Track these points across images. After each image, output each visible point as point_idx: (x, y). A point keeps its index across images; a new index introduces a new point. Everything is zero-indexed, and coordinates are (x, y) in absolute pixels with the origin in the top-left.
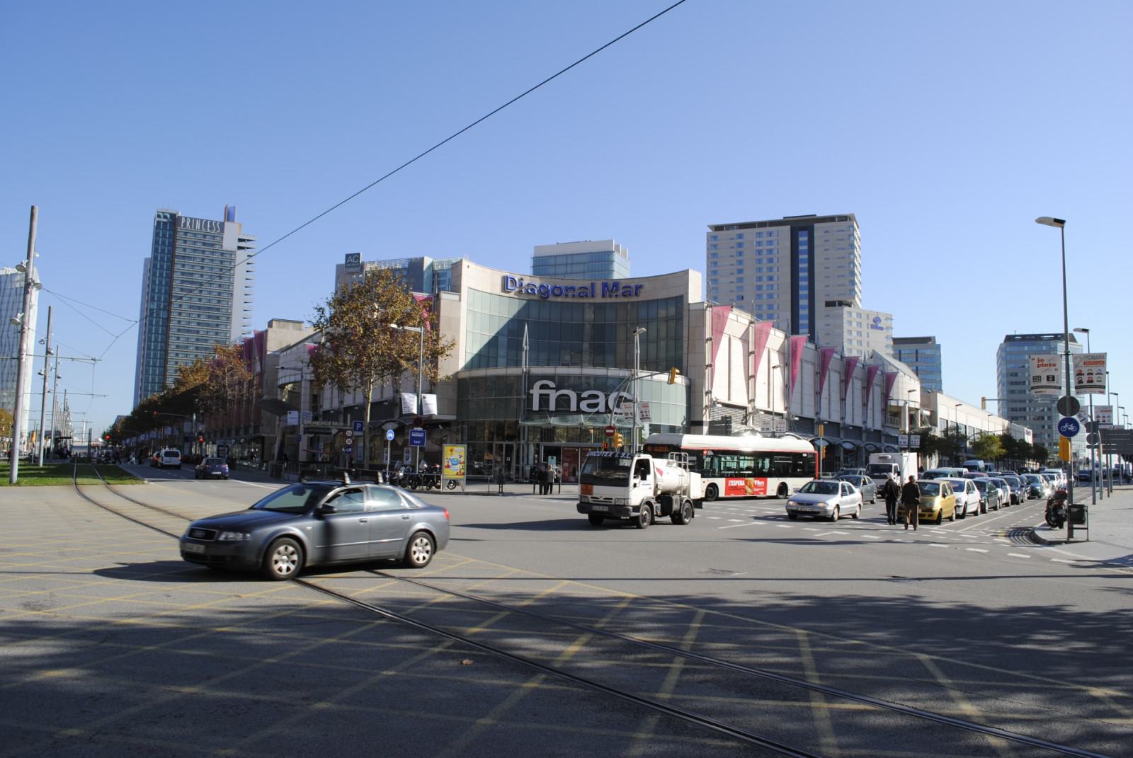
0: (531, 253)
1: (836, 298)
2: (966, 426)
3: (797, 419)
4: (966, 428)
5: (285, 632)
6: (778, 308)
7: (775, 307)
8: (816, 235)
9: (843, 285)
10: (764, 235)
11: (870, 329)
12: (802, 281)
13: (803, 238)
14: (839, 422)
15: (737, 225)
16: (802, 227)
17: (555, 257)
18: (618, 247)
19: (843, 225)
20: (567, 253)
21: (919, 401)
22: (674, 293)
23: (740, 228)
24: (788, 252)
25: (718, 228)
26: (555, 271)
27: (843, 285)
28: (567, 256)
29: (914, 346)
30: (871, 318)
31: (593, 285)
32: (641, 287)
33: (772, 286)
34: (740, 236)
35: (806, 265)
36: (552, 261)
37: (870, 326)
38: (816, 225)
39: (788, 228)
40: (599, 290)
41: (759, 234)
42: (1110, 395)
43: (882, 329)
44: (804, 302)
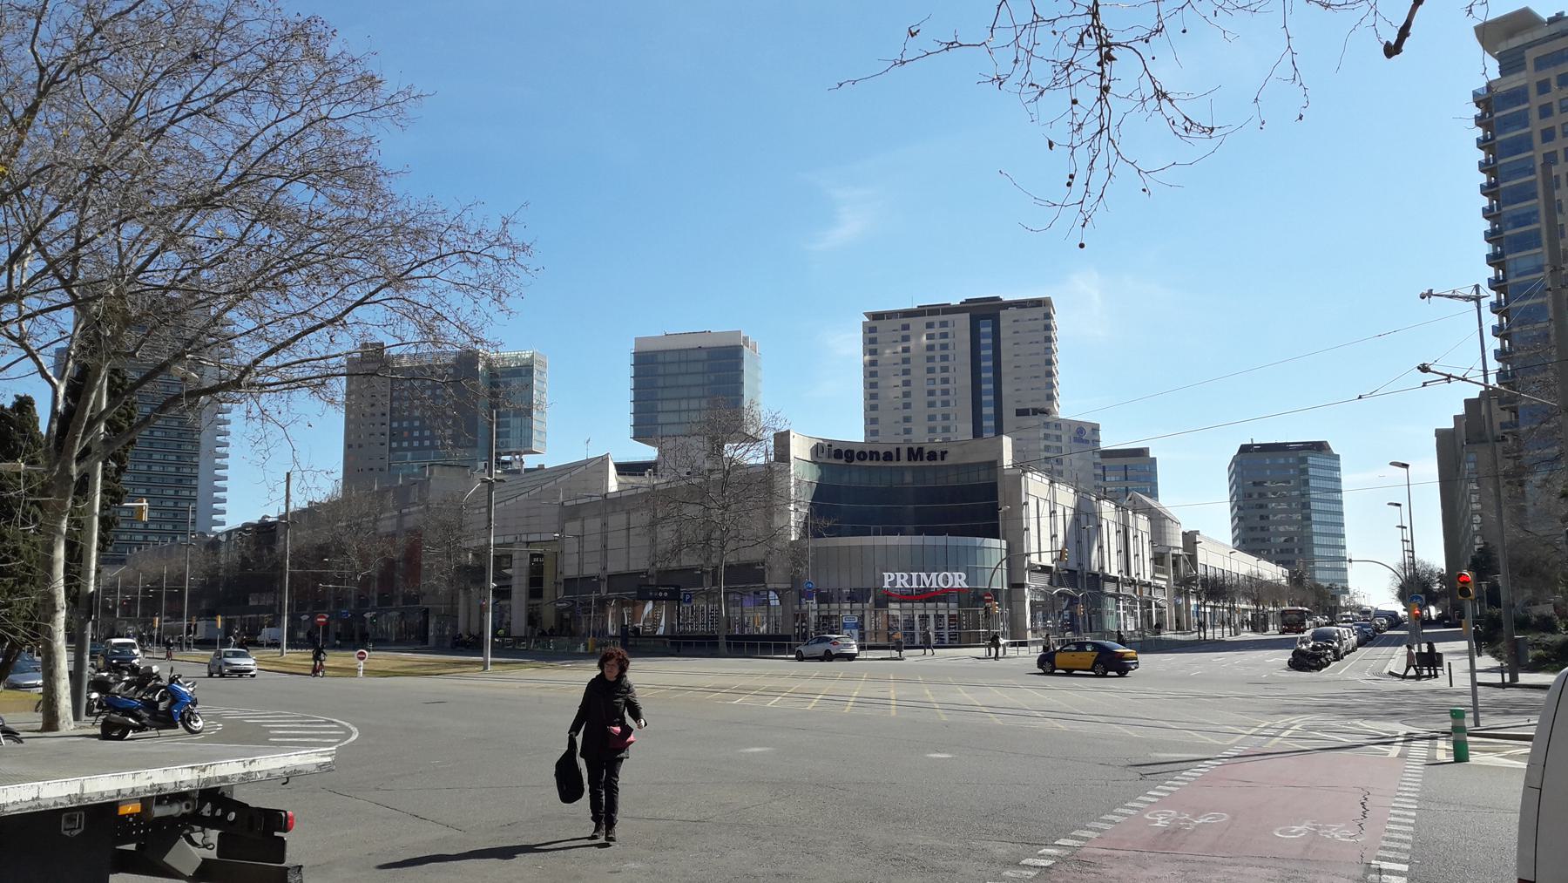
0: (631, 347)
1: (1030, 406)
2: (1206, 566)
3: (1067, 572)
4: (1206, 569)
5: (1050, 712)
6: (956, 418)
7: (952, 417)
8: (1002, 324)
9: (1038, 389)
10: (937, 325)
11: (1073, 443)
12: (985, 383)
13: (986, 329)
14: (1117, 575)
15: (900, 312)
16: (985, 312)
17: (664, 352)
18: (746, 339)
19: (1038, 312)
20: (679, 347)
21: (1181, 546)
22: (986, 457)
23: (904, 317)
24: (967, 347)
25: (876, 316)
26: (665, 370)
27: (1038, 389)
28: (679, 351)
29: (1122, 461)
30: (1074, 429)
31: (898, 449)
32: (946, 452)
33: (934, 379)
34: (906, 327)
35: (990, 364)
36: (660, 358)
37: (1072, 440)
38: (1002, 312)
39: (967, 315)
40: (904, 454)
41: (929, 325)
42: (1479, 688)
43: (1087, 442)
44: (988, 411)
